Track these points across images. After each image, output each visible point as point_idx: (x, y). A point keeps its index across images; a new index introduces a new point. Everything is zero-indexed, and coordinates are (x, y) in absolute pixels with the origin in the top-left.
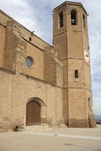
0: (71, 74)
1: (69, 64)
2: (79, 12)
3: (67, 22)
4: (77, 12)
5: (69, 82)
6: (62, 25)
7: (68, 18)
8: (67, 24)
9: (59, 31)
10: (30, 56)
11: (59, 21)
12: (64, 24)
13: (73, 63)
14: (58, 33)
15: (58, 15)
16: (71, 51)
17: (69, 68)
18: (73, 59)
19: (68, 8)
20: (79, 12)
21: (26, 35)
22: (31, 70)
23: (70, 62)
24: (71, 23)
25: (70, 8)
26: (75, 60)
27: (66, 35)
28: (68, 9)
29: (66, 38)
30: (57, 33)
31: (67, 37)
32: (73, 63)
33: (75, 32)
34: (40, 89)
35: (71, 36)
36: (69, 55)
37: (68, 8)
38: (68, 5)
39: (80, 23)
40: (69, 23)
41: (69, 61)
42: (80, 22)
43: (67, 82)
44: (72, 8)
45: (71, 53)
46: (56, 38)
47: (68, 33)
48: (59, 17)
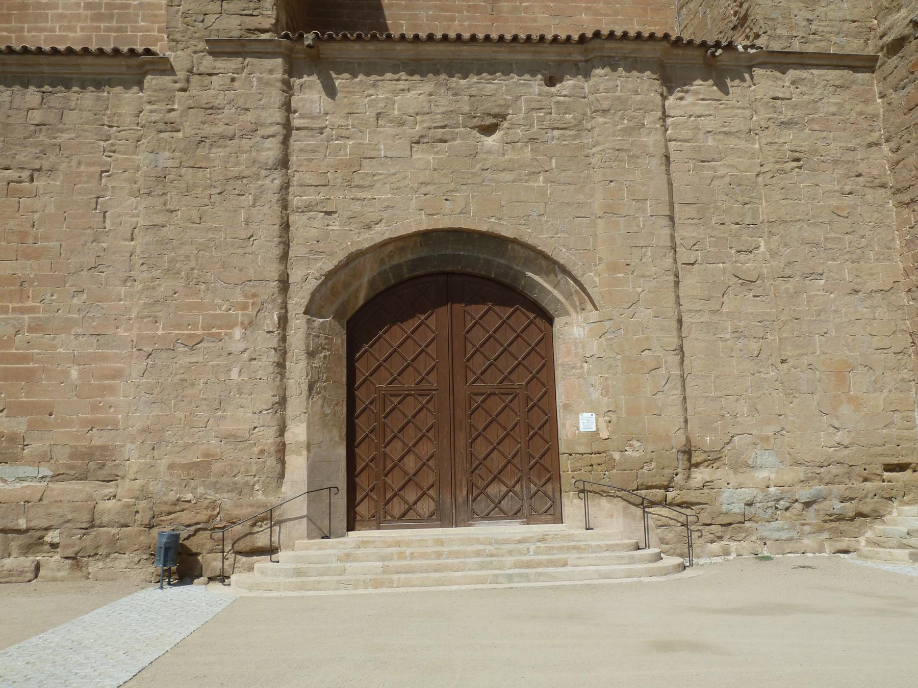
34: (490, 141)
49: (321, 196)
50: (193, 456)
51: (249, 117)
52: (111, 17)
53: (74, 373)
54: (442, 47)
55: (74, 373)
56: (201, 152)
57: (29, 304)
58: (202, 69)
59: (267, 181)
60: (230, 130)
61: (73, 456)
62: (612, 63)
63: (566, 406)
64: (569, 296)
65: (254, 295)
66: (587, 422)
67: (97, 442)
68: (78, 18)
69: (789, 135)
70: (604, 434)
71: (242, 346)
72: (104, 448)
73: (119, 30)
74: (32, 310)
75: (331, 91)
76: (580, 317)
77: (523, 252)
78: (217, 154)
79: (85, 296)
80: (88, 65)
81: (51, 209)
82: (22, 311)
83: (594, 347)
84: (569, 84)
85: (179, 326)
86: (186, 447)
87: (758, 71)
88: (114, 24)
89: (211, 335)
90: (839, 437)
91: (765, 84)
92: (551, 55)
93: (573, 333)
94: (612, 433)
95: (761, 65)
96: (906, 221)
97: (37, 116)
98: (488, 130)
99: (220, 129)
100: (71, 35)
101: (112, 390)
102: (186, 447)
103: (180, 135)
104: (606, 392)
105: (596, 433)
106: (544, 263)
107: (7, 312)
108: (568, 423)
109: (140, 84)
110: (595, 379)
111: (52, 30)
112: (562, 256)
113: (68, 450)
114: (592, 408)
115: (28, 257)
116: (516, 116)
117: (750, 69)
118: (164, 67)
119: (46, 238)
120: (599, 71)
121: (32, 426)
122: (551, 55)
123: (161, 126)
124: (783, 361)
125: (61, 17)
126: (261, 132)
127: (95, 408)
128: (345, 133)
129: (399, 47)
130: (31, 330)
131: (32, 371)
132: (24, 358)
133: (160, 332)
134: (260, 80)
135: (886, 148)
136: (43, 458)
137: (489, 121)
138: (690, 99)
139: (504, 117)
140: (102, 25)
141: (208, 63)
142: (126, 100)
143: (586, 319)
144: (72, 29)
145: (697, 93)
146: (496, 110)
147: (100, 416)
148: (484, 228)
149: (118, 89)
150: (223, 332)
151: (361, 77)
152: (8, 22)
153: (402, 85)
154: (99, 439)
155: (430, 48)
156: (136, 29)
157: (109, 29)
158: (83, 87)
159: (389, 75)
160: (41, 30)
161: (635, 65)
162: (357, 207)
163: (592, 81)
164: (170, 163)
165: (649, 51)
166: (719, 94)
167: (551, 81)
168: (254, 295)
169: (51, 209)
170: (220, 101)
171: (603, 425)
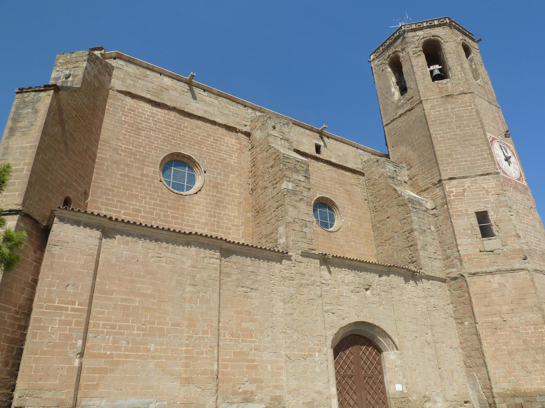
0: (464, 229)
1: (450, 196)
2: (447, 42)
3: (417, 77)
4: (443, 41)
5: (465, 256)
6: (403, 90)
7: (418, 66)
8: (418, 82)
9: (398, 108)
10: (323, 197)
11: (393, 79)
12: (409, 84)
13: (464, 190)
14: (396, 114)
15: (387, 66)
16: (450, 155)
17: (454, 208)
18: (460, 178)
19: (412, 40)
20: (447, 42)
21: (304, 141)
22: (332, 235)
23: (452, 192)
24: (429, 78)
25: (417, 38)
26: (467, 183)
27: (422, 114)
28: (413, 43)
29: (424, 121)
30: (394, 114)
31: (428, 117)
32: (464, 190)
33: (449, 99)
34: (368, 292)
35: (439, 111)
36: (432, 125)
37: (412, 40)
38: (411, 34)
39: (459, 69)
40: (424, 79)
41: (447, 187)
42: (459, 67)
43: (455, 258)
44: (423, 38)
45: (452, 163)
46: (394, 128)
47: (427, 106)
48: (389, 70)
49: (331, 307)
50: (309, 400)
51: (312, 278)
52: (215, 216)
53: (269, 367)
54: (357, 263)
55: (269, 367)
56: (301, 289)
57: (253, 339)
58: (299, 261)
59: (318, 301)
60: (309, 282)
61: (271, 399)
62: (395, 273)
63: (390, 382)
64: (389, 345)
65: (320, 341)
66: (399, 387)
67: (278, 394)
68: (203, 214)
69: (432, 300)
70: (405, 391)
71: (318, 359)
72: (280, 396)
73: (218, 222)
74: (255, 342)
75: (330, 272)
76: (393, 352)
77: (378, 330)
78: (305, 290)
79: (270, 338)
80: (266, 253)
81: (258, 304)
82: (251, 342)
83: (399, 362)
84: (384, 278)
85: (301, 351)
86: (306, 396)
87: (423, 280)
88: (216, 219)
89: (310, 355)
90: (455, 392)
91: (426, 284)
92: (380, 268)
93: (390, 357)
94: (408, 391)
95: (424, 278)
96: (460, 328)
97: (251, 269)
98: (367, 290)
99: (305, 282)
100: (201, 220)
101: (280, 374)
102: (306, 396)
103: (294, 282)
104: (404, 377)
105: (403, 391)
106: (383, 334)
107: (247, 342)
108: (391, 387)
109: (281, 263)
110: (401, 373)
111: (194, 217)
112: (389, 333)
113: (269, 398)
114: (400, 383)
115: (252, 321)
116: (374, 286)
117: (421, 279)
118: (289, 258)
119: (257, 315)
120: (392, 275)
121: (258, 387)
122: (380, 268)
123: (290, 278)
124: (439, 369)
125: (197, 213)
126: (316, 284)
127: (276, 381)
128: (335, 287)
129: (347, 261)
130: (255, 350)
131: (256, 366)
132: (253, 361)
133: (296, 353)
134: (314, 266)
135: (451, 306)
136: (261, 401)
137: (367, 287)
138: (410, 286)
139: (371, 286)
140: (212, 219)
141: (300, 258)
142: (276, 267)
143: (395, 353)
144: (201, 218)
145: (411, 284)
146: (369, 284)
147: (278, 384)
148: (371, 322)
149: (274, 263)
150: (313, 353)
151: (337, 268)
152: (178, 211)
153: (347, 273)
154: (278, 393)
155: (354, 262)
156: (223, 223)
157: (214, 221)
158: (264, 261)
159: (343, 269)
160: (191, 217)
161: (400, 275)
162: (340, 312)
163: (390, 278)
164: (293, 292)
165: (403, 271)
166: (416, 285)
167: (380, 276)
168: (320, 341)
169: (258, 304)
170: (305, 271)
171: (405, 389)
